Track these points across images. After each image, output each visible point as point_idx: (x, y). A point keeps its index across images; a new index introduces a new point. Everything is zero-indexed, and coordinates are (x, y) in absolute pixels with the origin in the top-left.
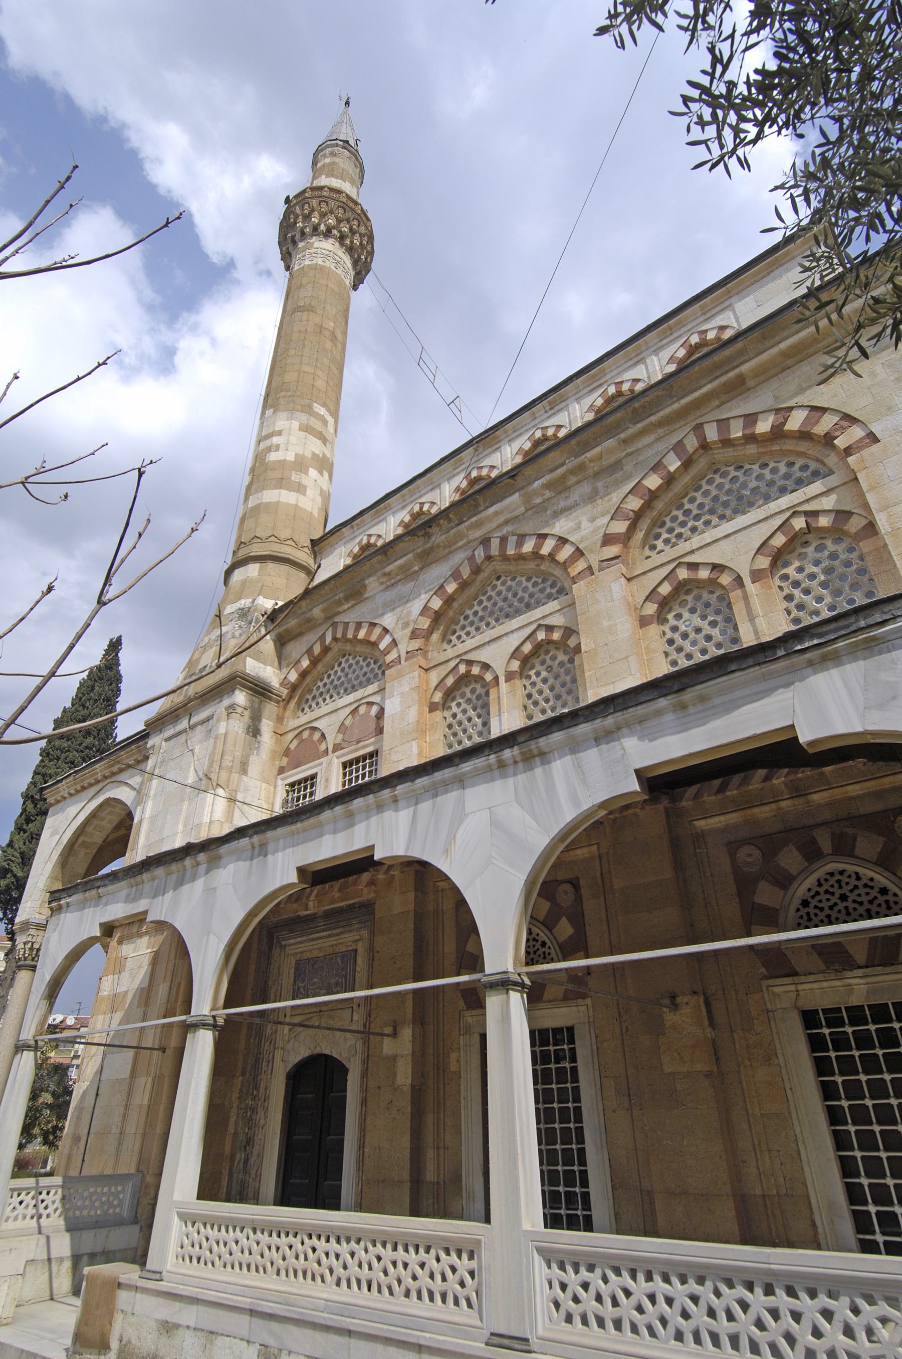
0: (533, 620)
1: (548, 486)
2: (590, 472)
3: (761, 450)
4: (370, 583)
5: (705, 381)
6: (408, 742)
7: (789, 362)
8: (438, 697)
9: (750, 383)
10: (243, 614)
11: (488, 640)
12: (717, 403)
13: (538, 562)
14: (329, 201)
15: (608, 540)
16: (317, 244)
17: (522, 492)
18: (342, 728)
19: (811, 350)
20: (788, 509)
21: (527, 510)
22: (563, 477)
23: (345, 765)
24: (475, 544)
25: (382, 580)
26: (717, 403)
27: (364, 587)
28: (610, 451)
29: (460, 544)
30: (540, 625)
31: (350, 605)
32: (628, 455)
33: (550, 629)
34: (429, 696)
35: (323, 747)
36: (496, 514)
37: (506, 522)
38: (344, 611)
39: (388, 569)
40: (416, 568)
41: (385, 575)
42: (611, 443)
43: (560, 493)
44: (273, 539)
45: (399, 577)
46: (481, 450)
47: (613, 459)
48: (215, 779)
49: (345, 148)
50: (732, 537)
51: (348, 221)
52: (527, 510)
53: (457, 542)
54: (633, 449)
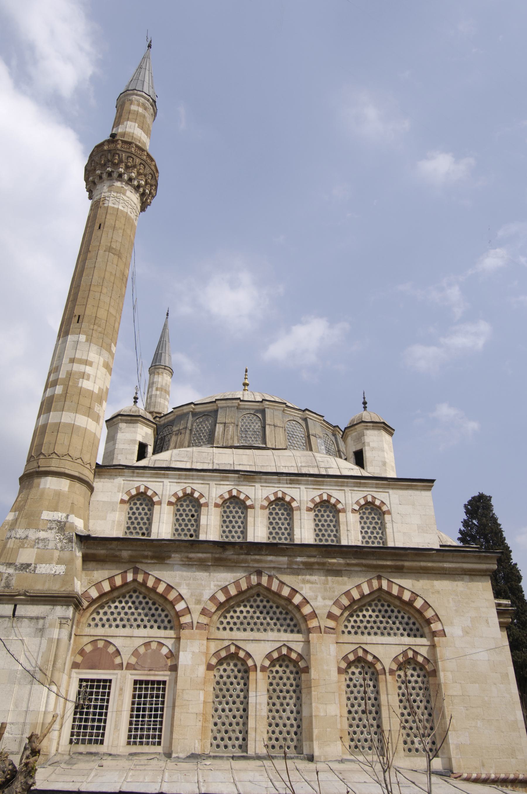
0: (282, 639)
1: (304, 563)
2: (326, 568)
3: (401, 605)
4: (174, 557)
5: (389, 558)
6: (197, 689)
7: (421, 571)
8: (214, 661)
9: (405, 571)
10: (62, 527)
11: (252, 638)
12: (390, 570)
13: (288, 603)
14: (147, 166)
15: (330, 616)
16: (128, 193)
17: (290, 559)
18: (136, 653)
19: (430, 572)
20: (408, 645)
21: (287, 568)
22: (312, 564)
23: (136, 682)
24: (252, 570)
25: (183, 559)
26: (390, 570)
27: (169, 557)
28: (339, 564)
29: (243, 565)
30: (284, 645)
31: (153, 561)
32: (346, 570)
33: (290, 649)
34: (208, 659)
35: (117, 661)
36: (271, 561)
37: (274, 568)
38: (146, 563)
39: (192, 555)
40: (210, 564)
41: (187, 557)
42: (341, 561)
43: (307, 569)
44: (79, 461)
45: (196, 563)
46: (242, 479)
47: (339, 568)
48: (50, 676)
49: (152, 106)
50: (385, 646)
51: (145, 175)
52: (287, 568)
53: (241, 563)
54: (349, 569)
